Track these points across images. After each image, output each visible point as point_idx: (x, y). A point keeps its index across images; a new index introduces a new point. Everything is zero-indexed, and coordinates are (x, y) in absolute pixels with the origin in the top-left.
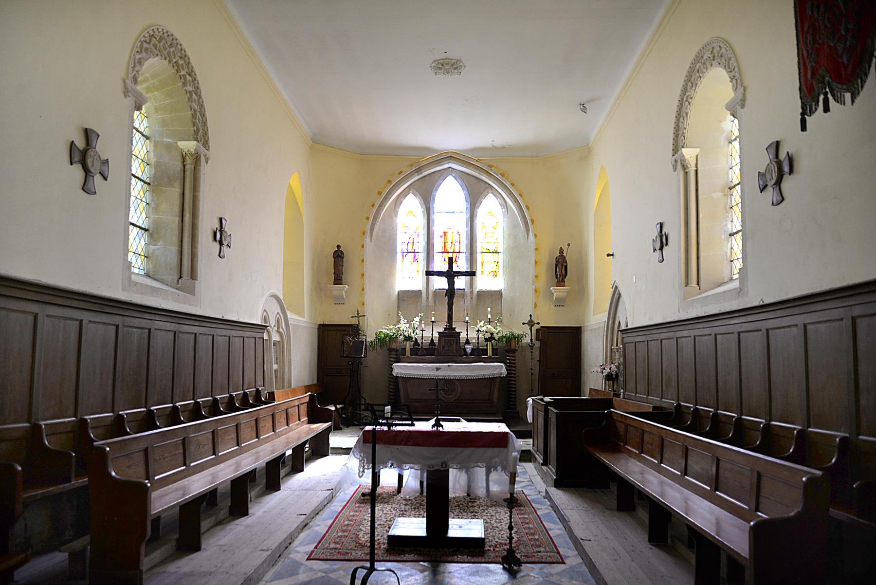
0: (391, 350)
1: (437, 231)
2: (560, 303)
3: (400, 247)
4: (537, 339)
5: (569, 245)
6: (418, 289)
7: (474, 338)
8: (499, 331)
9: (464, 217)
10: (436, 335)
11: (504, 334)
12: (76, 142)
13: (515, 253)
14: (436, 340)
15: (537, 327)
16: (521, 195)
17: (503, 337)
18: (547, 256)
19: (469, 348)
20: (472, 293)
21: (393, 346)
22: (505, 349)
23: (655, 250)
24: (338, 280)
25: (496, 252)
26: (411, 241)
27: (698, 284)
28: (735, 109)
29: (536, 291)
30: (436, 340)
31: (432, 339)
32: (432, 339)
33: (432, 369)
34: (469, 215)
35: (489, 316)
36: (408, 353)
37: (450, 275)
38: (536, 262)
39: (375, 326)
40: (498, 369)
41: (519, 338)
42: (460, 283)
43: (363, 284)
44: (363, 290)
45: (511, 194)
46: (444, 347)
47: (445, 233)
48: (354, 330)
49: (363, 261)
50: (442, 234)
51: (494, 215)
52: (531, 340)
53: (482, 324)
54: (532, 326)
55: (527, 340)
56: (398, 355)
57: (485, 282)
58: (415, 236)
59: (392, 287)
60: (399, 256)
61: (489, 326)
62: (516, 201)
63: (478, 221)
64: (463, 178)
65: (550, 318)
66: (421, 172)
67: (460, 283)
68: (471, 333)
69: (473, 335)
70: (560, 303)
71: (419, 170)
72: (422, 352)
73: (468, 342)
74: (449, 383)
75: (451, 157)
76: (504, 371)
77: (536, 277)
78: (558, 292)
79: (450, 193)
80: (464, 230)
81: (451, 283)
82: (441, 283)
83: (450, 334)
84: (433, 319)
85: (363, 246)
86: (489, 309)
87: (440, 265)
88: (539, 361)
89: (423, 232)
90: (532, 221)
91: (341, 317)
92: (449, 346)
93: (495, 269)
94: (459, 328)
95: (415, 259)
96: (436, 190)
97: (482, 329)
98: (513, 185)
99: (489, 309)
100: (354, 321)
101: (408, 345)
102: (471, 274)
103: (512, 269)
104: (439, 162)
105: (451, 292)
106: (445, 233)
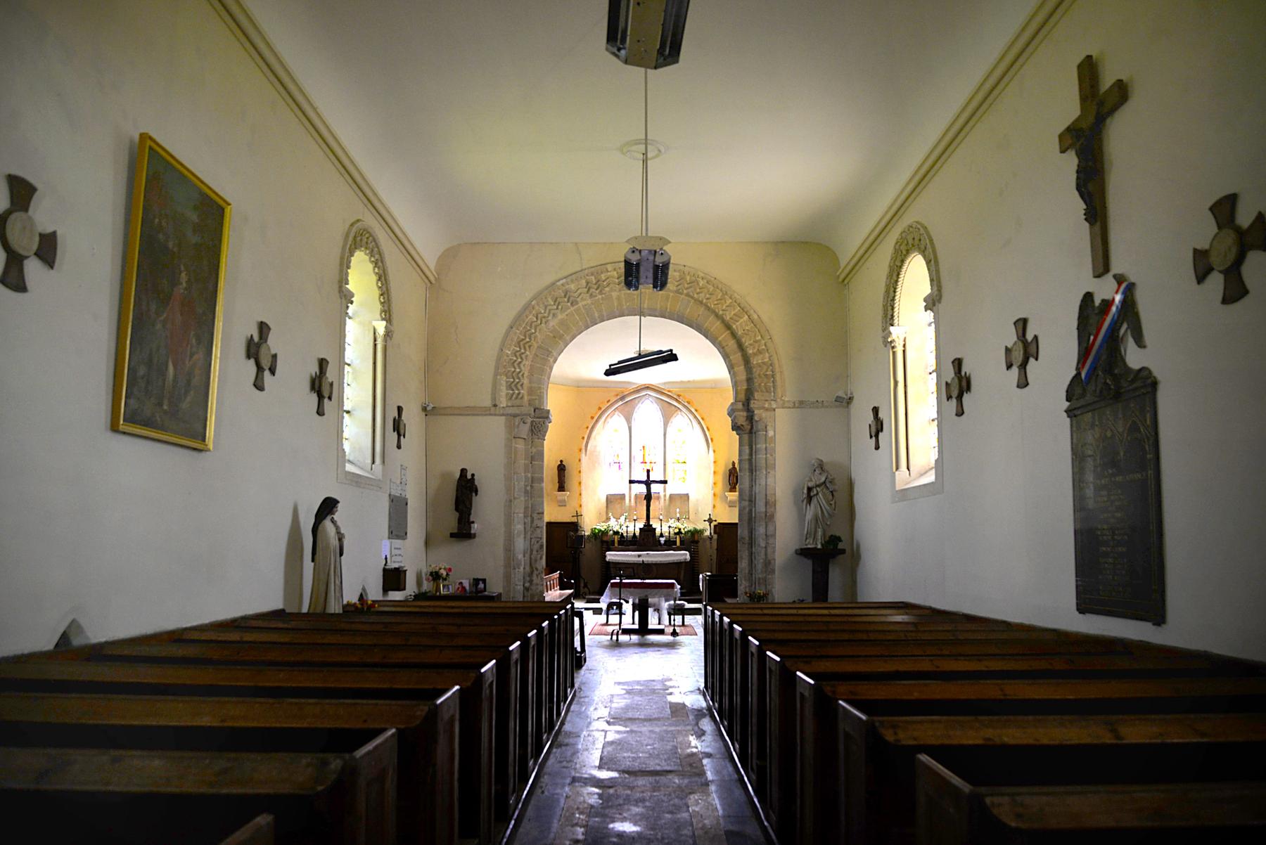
0: (603, 542)
8: (686, 526)
19: (662, 540)
22: (690, 540)
24: (561, 488)
37: (648, 483)
39: (591, 522)
40: (684, 555)
48: (574, 526)
55: (707, 533)
57: (672, 488)
68: (664, 528)
69: (665, 530)
73: (662, 535)
76: (688, 557)
83: (648, 529)
92: (647, 539)
94: (655, 524)
100: (574, 520)
101: (616, 538)
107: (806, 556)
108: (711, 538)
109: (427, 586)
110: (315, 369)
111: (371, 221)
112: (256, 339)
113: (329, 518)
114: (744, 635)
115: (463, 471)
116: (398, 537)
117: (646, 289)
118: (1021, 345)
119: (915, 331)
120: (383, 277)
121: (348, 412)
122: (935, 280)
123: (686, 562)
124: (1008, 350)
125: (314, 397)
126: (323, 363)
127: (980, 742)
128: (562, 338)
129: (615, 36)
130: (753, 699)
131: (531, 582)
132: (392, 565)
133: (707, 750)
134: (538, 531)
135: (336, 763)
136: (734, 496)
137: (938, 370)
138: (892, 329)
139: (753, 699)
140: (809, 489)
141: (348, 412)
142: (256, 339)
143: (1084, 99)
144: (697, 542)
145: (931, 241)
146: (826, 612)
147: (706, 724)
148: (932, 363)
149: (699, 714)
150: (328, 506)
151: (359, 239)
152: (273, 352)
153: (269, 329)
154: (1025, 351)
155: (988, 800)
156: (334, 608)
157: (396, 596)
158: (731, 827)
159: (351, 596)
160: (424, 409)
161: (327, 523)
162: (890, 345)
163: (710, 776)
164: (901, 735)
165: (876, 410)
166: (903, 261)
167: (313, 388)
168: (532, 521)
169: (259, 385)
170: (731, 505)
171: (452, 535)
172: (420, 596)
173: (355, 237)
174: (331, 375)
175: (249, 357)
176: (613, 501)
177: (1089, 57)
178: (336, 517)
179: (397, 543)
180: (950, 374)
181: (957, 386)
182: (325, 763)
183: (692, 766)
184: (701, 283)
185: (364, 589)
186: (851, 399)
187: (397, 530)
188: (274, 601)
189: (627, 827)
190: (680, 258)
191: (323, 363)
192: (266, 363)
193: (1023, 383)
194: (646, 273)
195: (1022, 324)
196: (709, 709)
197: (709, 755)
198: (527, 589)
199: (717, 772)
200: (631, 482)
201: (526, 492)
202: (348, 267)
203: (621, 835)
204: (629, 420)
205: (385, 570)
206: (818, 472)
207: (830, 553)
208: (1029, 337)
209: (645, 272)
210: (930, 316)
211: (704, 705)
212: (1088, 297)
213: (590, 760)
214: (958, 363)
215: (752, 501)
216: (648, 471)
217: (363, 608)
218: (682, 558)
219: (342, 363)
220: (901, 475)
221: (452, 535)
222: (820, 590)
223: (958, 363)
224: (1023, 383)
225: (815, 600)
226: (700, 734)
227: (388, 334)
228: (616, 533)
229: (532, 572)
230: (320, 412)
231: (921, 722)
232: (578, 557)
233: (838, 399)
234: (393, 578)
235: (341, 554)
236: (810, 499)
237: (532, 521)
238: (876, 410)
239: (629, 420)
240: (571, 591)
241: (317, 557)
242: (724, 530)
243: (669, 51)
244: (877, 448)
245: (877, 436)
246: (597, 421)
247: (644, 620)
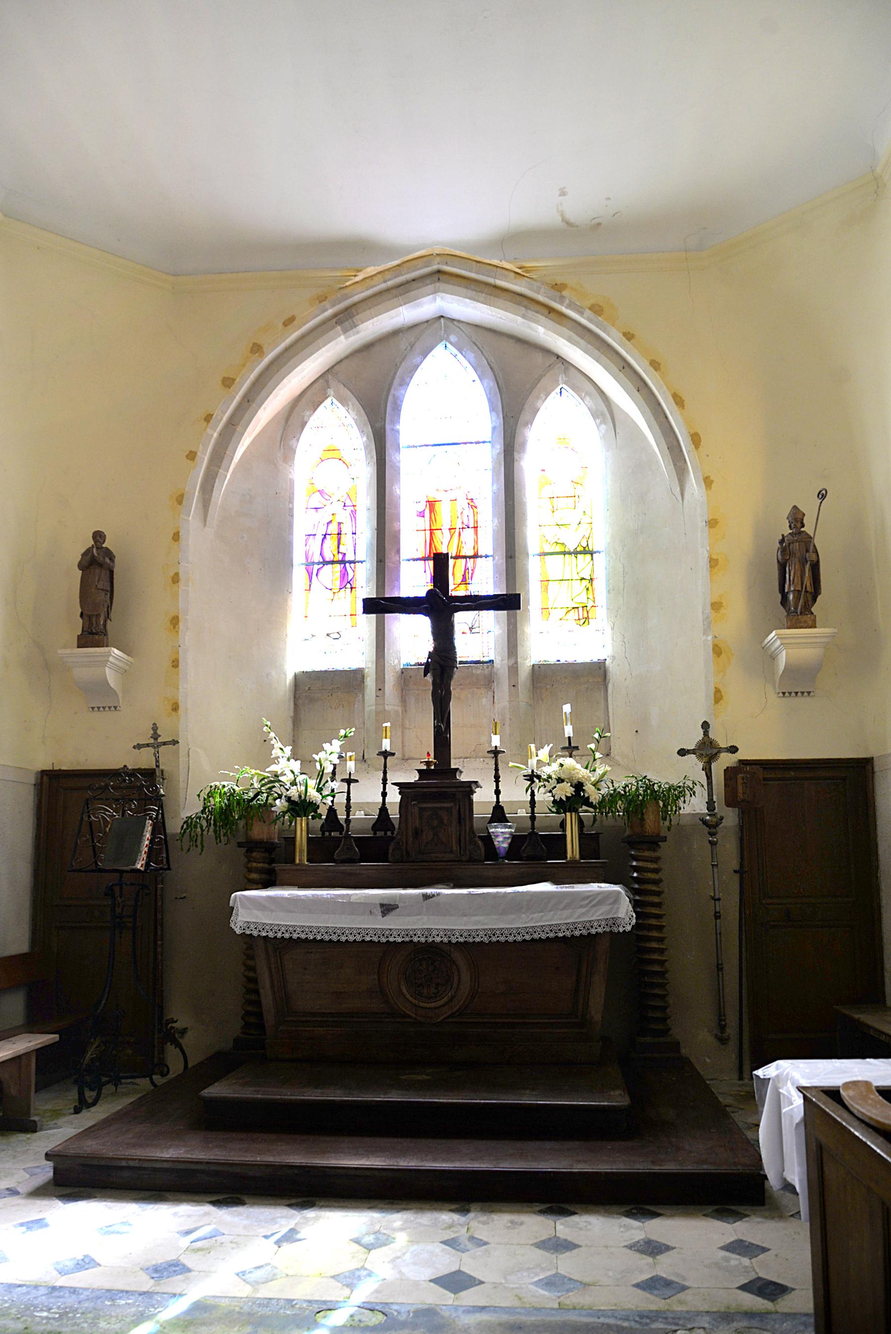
0: (251, 846)
1: (409, 496)
2: (798, 685)
3: (301, 549)
4: (731, 800)
5: (822, 495)
6: (354, 666)
7: (520, 804)
8: (602, 776)
9: (484, 460)
10: (394, 797)
11: (619, 785)
13: (640, 548)
14: (394, 813)
15: (726, 761)
16: (655, 365)
17: (614, 796)
18: (750, 532)
19: (501, 835)
20: (514, 669)
21: (259, 831)
22: (620, 835)
24: (93, 633)
25: (585, 552)
26: (333, 529)
29: (717, 651)
30: (394, 813)
31: (383, 810)
32: (383, 810)
33: (365, 907)
34: (499, 447)
35: (569, 730)
36: (301, 856)
37: (440, 606)
38: (713, 563)
40: (601, 903)
41: (675, 794)
42: (477, 637)
43: (176, 649)
44: (175, 664)
45: (624, 369)
46: (417, 833)
47: (431, 504)
48: (140, 788)
49: (176, 579)
50: (422, 506)
51: (575, 449)
52: (710, 805)
53: (544, 754)
55: (695, 805)
56: (269, 863)
57: (551, 638)
58: (344, 516)
59: (273, 659)
60: (299, 574)
61: (569, 762)
62: (641, 388)
63: (528, 464)
64: (483, 342)
65: (766, 734)
66: (346, 312)
67: (477, 637)
68: (507, 787)
69: (514, 794)
70: (798, 685)
71: (346, 318)
72: (343, 850)
73: (499, 814)
74: (427, 959)
75: (439, 271)
76: (625, 913)
77: (716, 606)
78: (789, 645)
79: (445, 395)
80: (486, 489)
81: (444, 635)
83: (439, 790)
84: (386, 745)
85: (176, 537)
86: (567, 708)
87: (415, 581)
88: (740, 872)
89: (366, 502)
90: (696, 440)
91: (104, 746)
92: (431, 832)
93: (582, 599)
94: (469, 768)
95: (346, 582)
96: (404, 383)
97: (546, 771)
98: (629, 336)
99: (567, 708)
100: (145, 760)
101: (301, 828)
102: (508, 602)
103: (635, 598)
104: (404, 289)
105: (442, 662)
106: (431, 504)
108: (710, 824)
123: (614, 938)
144: (654, 842)
176: (321, 696)
185: (630, 1247)
218: (593, 918)
228: (301, 807)
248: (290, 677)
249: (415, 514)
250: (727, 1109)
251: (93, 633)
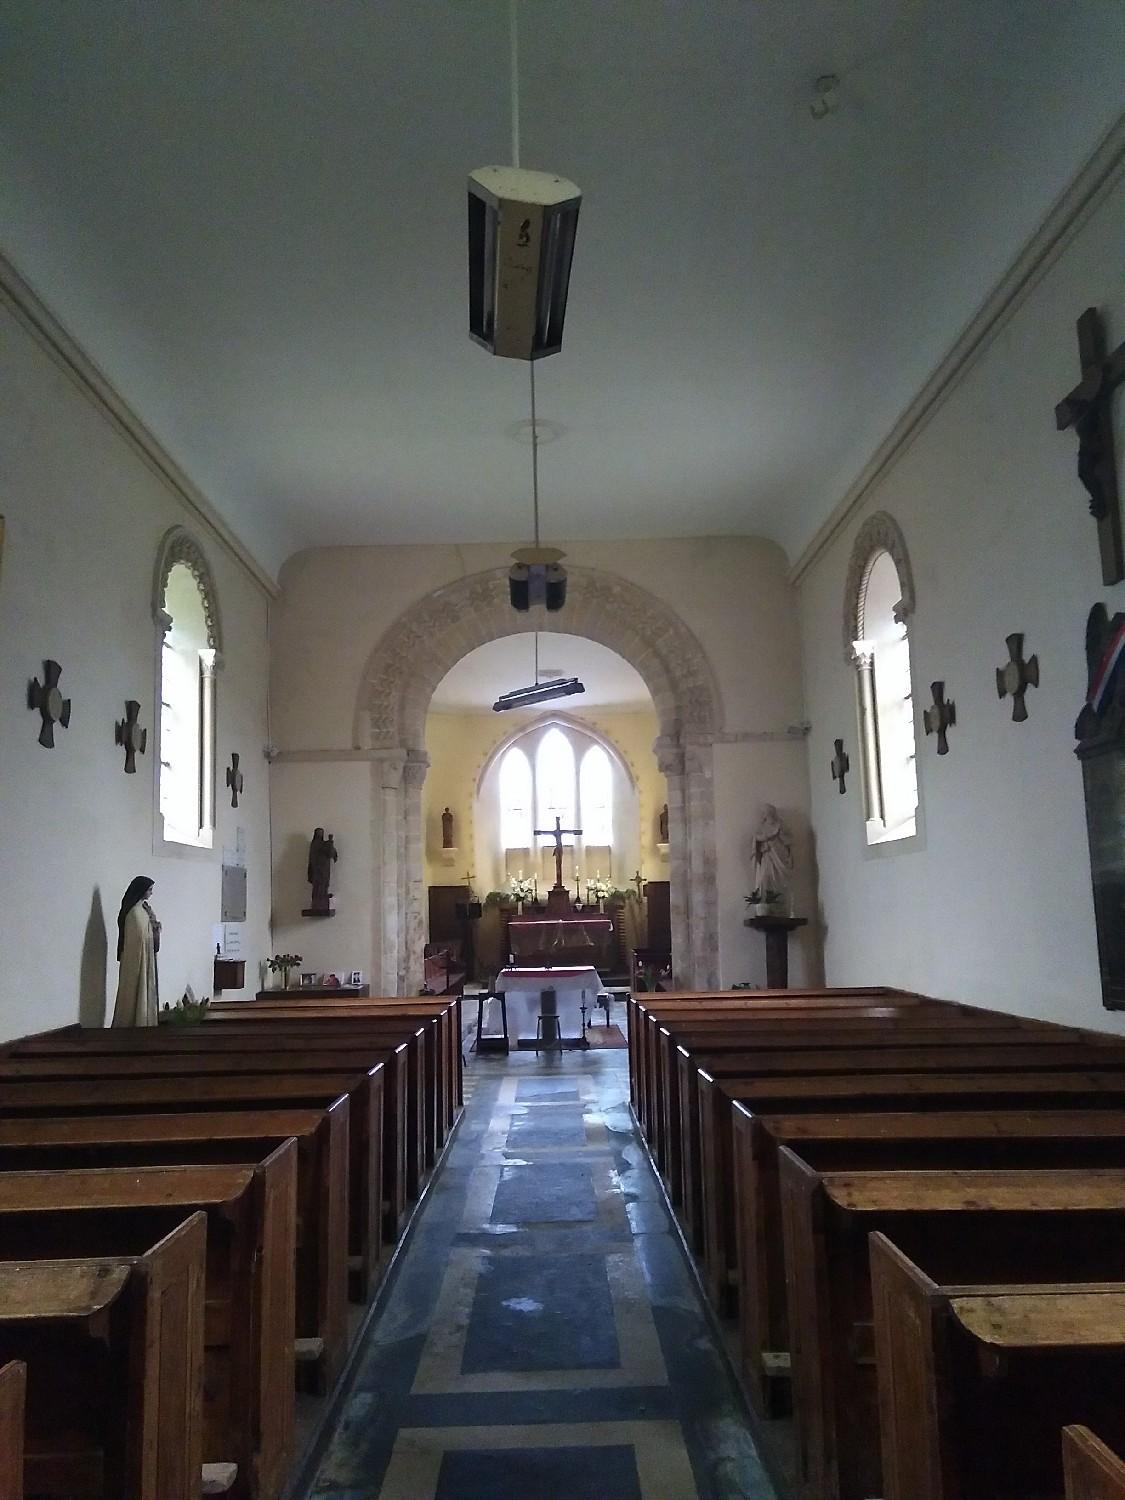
12: (565, 559)
15: (644, 883)
19: (579, 906)
21: (506, 906)
23: (834, 777)
24: (448, 843)
27: (882, 817)
28: (903, 613)
35: (598, 876)
37: (558, 833)
39: (483, 887)
42: (567, 840)
54: (640, 882)
57: (587, 840)
69: (583, 893)
73: (578, 900)
82: (551, 841)
83: (559, 892)
94: (568, 885)
102: (578, 833)
105: (558, 851)
107: (757, 928)
109: (272, 980)
110: (121, 715)
111: (193, 528)
112: (42, 682)
113: (141, 902)
114: (672, 1041)
115: (318, 833)
116: (235, 919)
117: (538, 609)
118: (1014, 667)
119: (886, 650)
120: (210, 595)
121: (167, 764)
122: (907, 584)
124: (1000, 674)
125: (122, 750)
126: (132, 708)
127: (959, 1207)
128: (441, 664)
129: (480, 326)
130: (685, 1120)
131: (407, 969)
132: (225, 957)
133: (632, 1190)
134: (415, 904)
135: (120, 1272)
136: (664, 847)
137: (914, 695)
138: (855, 644)
139: (685, 1120)
140: (759, 844)
141: (167, 764)
142: (42, 682)
143: (1086, 363)
145: (901, 536)
146: (781, 1003)
147: (632, 1154)
148: (906, 687)
149: (621, 1137)
150: (140, 889)
151: (176, 548)
152: (65, 697)
153: (60, 669)
154: (1020, 676)
155: (956, 1304)
156: (147, 1017)
157: (230, 995)
158: (662, 1302)
159: (170, 995)
160: (267, 755)
161: (139, 910)
162: (854, 662)
163: (634, 1227)
164: (857, 1197)
165: (839, 744)
166: (866, 561)
167: (119, 739)
168: (408, 892)
169: (46, 740)
170: (665, 858)
171: (305, 913)
172: (263, 995)
173: (172, 548)
174: (143, 720)
175: (31, 705)
177: (1091, 311)
178: (150, 901)
179: (233, 926)
180: (929, 702)
181: (937, 717)
182: (105, 1271)
183: (611, 1213)
184: (617, 589)
185: (189, 989)
186: (807, 730)
187: (233, 909)
188: (64, 1012)
189: (526, 1305)
190: (576, 566)
191: (132, 708)
192: (55, 711)
193: (1020, 714)
194: (536, 588)
195: (1016, 642)
196: (636, 1131)
197: (631, 1197)
198: (401, 979)
199: (645, 1219)
200: (537, 833)
201: (399, 856)
202: (166, 585)
203: (519, 1315)
204: (531, 755)
205: (217, 963)
206: (769, 821)
207: (787, 925)
208: (1026, 658)
209: (538, 589)
210: (901, 629)
211: (630, 1126)
212: (1098, 611)
213: (481, 1203)
214: (938, 688)
215: (686, 858)
216: (558, 819)
217: (189, 1013)
219: (157, 703)
220: (874, 826)
221: (305, 913)
222: (777, 975)
223: (938, 688)
224: (1020, 714)
225: (772, 985)
226: (624, 1167)
227: (218, 665)
229: (408, 957)
230: (130, 768)
231: (882, 1179)
232: (469, 933)
233: (792, 730)
234: (227, 973)
235: (156, 949)
236: (759, 856)
237: (408, 892)
238: (839, 744)
239: (531, 755)
240: (461, 975)
241: (125, 954)
242: (658, 892)
243: (547, 340)
244: (843, 791)
245: (842, 777)
246: (491, 758)
247: (549, 1023)
248: (504, 851)
249: (742, 921)
250: (951, 1301)
251: (448, 843)
